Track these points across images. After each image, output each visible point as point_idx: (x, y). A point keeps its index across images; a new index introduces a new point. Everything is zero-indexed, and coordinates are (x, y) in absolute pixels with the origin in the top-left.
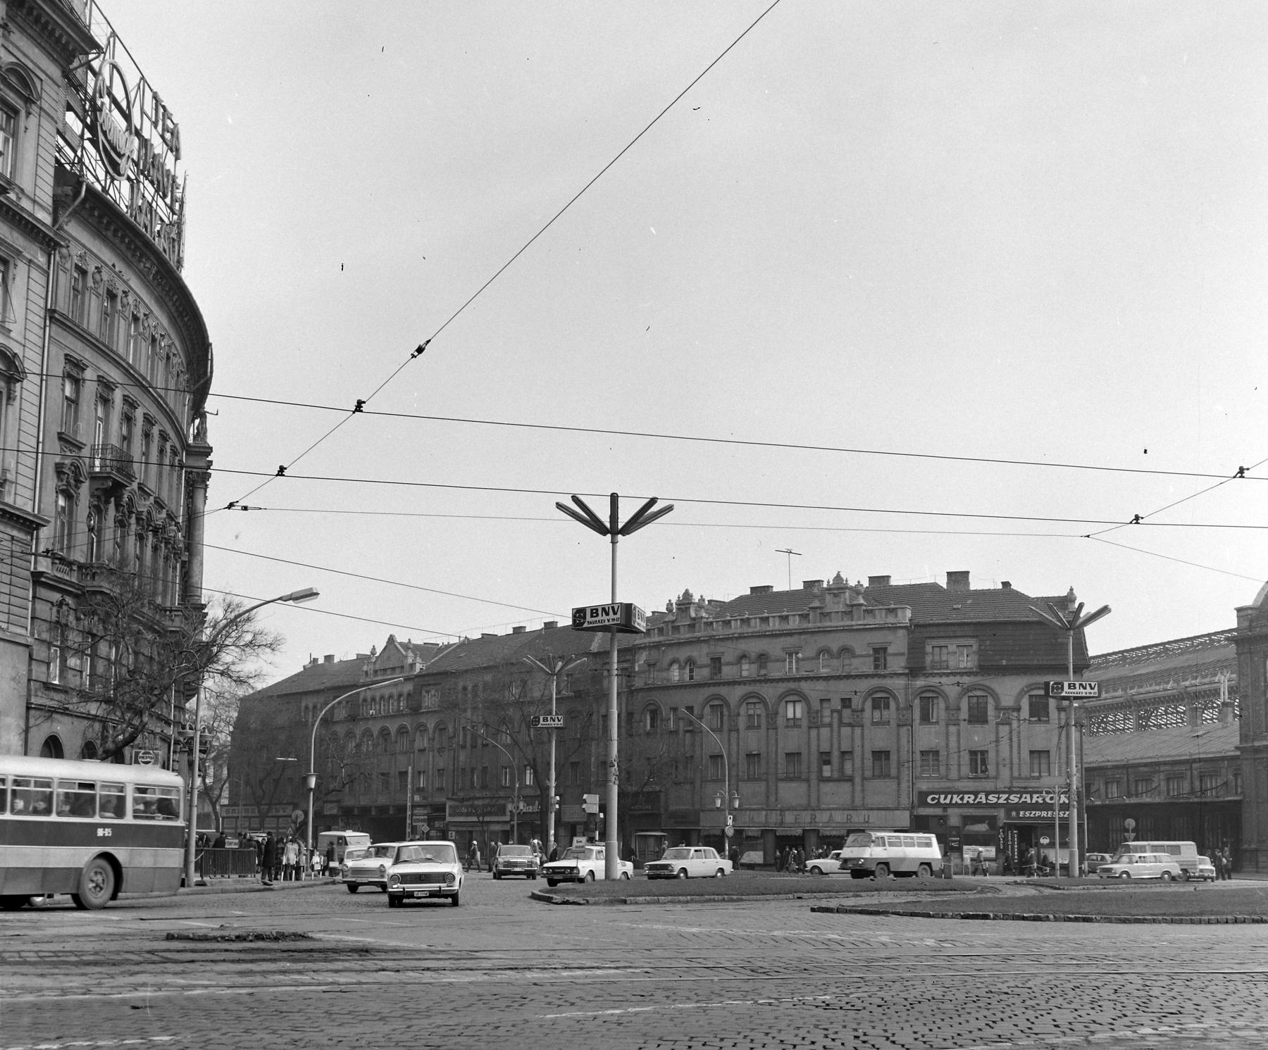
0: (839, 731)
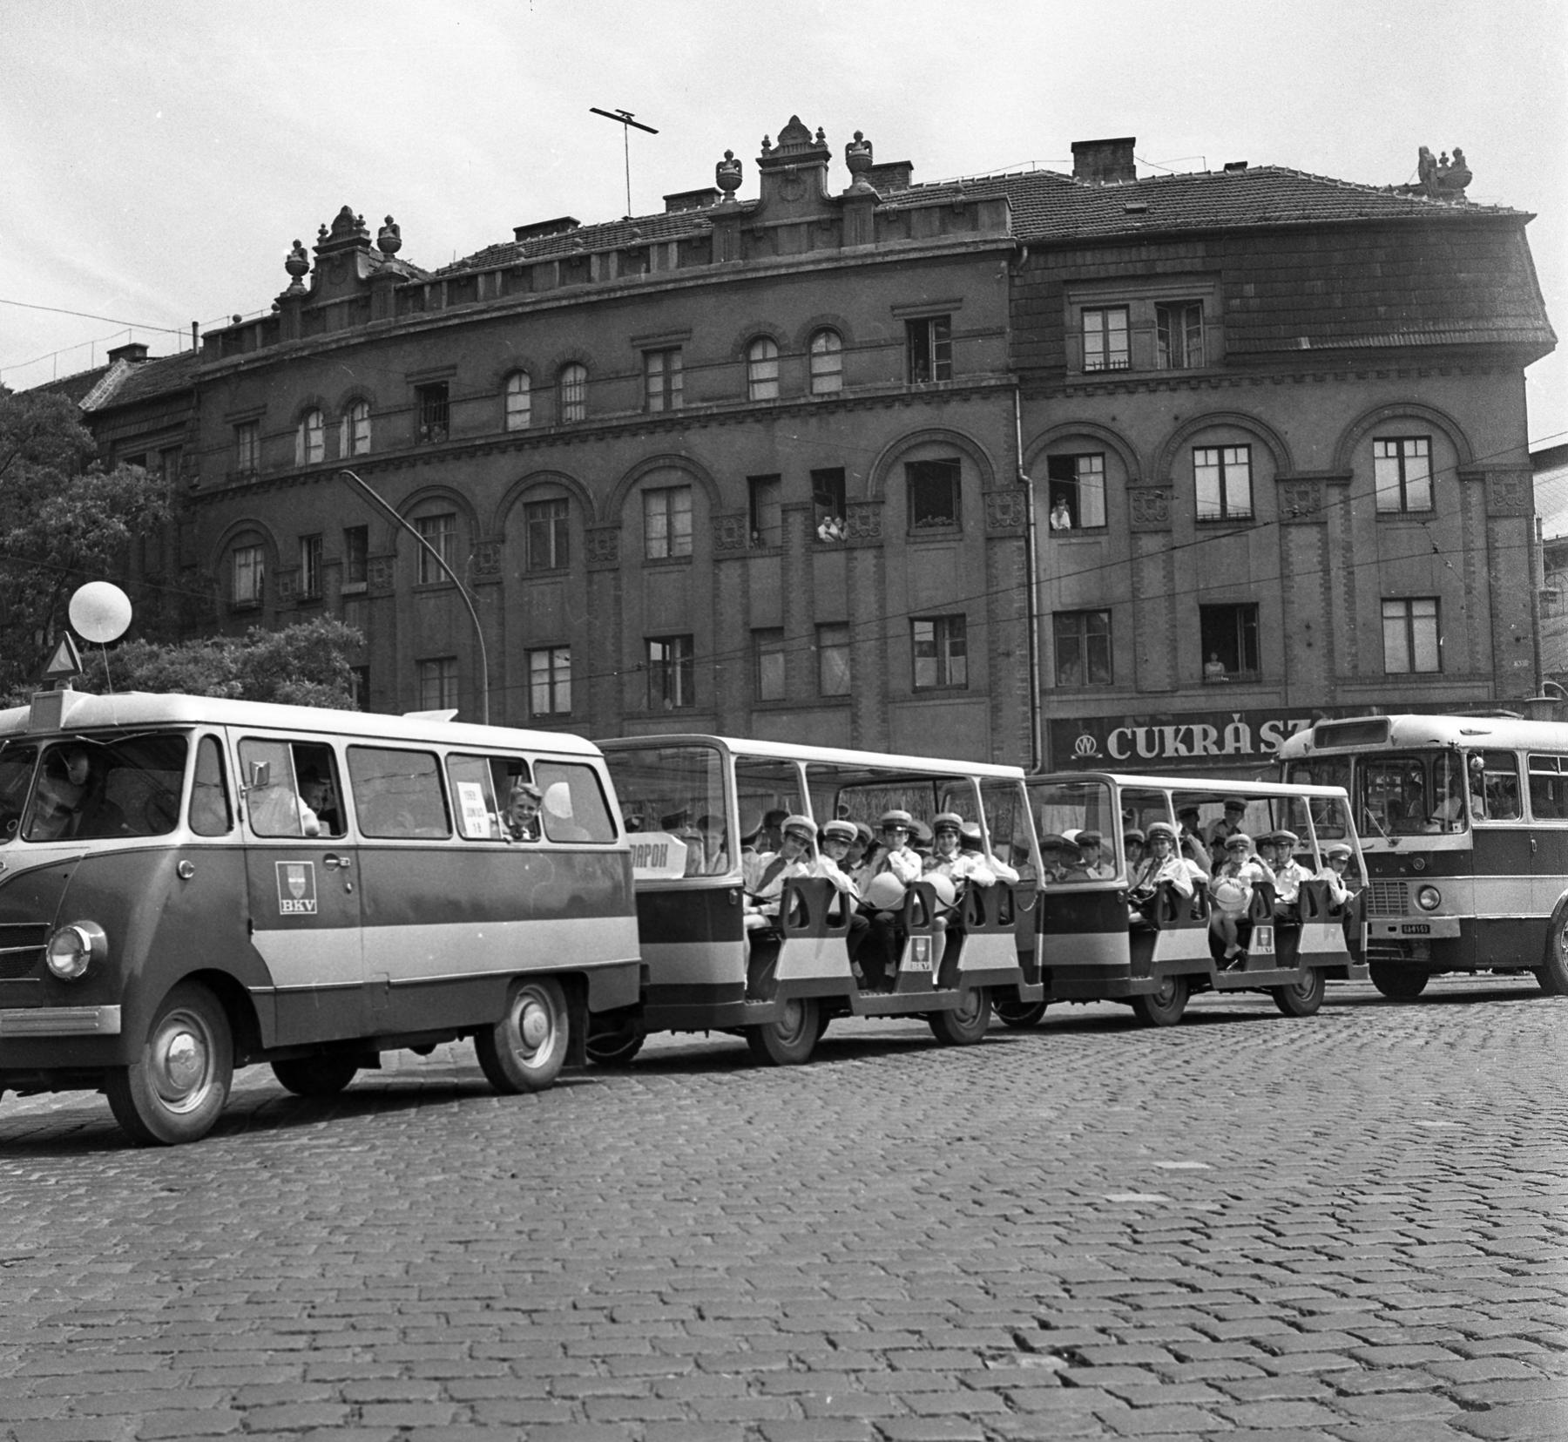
0: (809, 564)
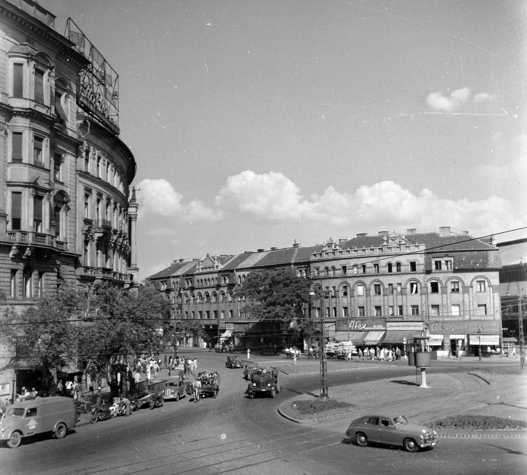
0: (397, 297)
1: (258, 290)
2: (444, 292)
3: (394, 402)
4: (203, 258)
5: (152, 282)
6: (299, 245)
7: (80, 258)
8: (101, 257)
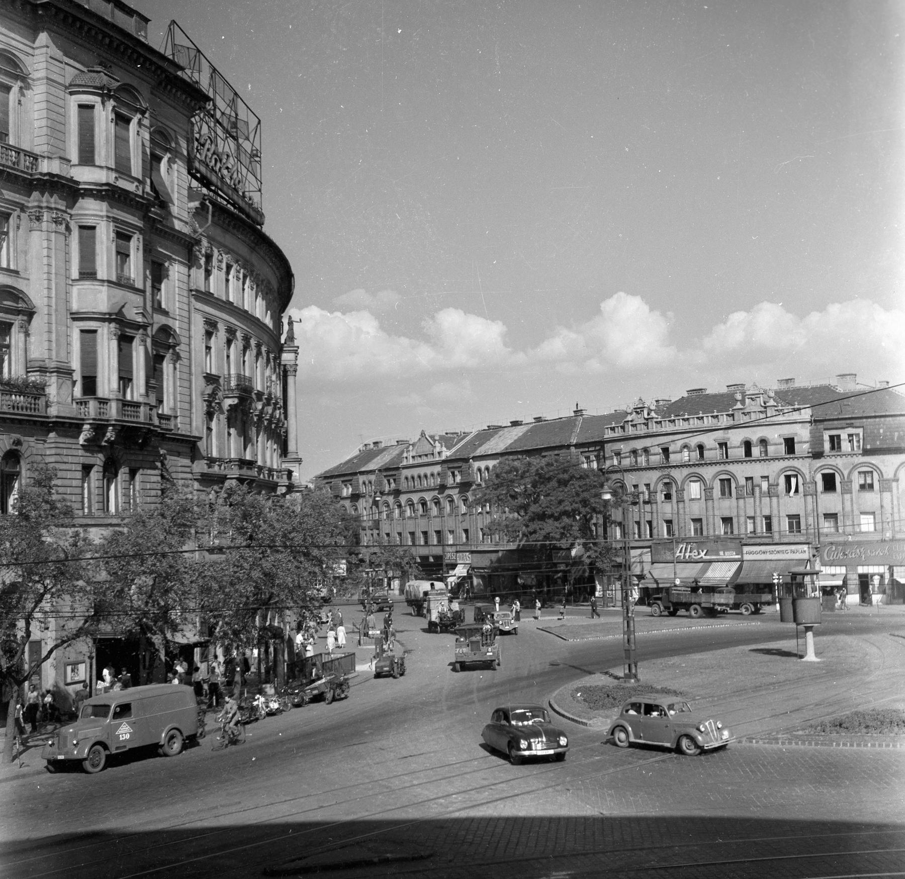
1: (513, 493)
2: (847, 490)
3: (756, 687)
4: (415, 438)
5: (327, 483)
6: (584, 413)
7: (199, 444)
8: (235, 441)
